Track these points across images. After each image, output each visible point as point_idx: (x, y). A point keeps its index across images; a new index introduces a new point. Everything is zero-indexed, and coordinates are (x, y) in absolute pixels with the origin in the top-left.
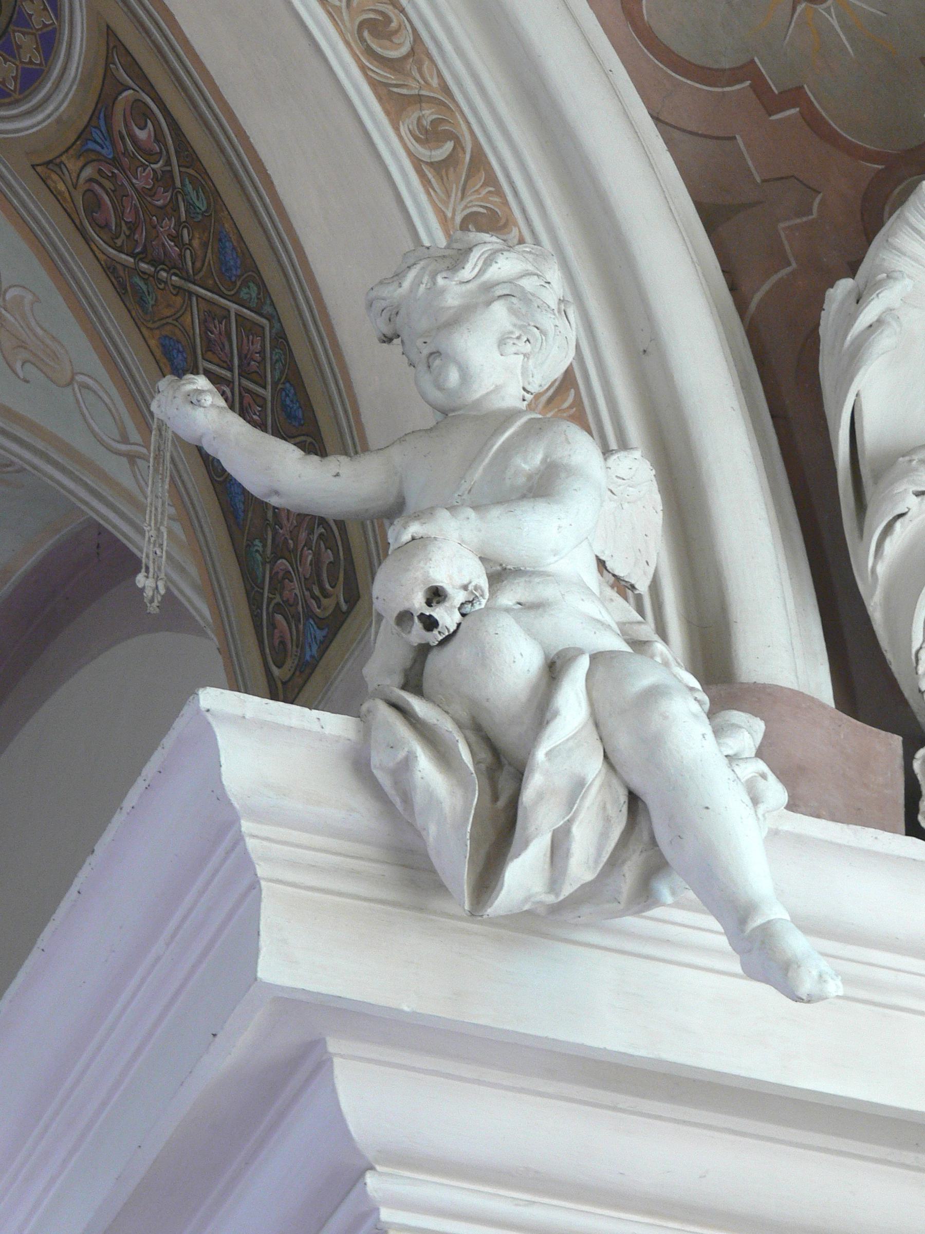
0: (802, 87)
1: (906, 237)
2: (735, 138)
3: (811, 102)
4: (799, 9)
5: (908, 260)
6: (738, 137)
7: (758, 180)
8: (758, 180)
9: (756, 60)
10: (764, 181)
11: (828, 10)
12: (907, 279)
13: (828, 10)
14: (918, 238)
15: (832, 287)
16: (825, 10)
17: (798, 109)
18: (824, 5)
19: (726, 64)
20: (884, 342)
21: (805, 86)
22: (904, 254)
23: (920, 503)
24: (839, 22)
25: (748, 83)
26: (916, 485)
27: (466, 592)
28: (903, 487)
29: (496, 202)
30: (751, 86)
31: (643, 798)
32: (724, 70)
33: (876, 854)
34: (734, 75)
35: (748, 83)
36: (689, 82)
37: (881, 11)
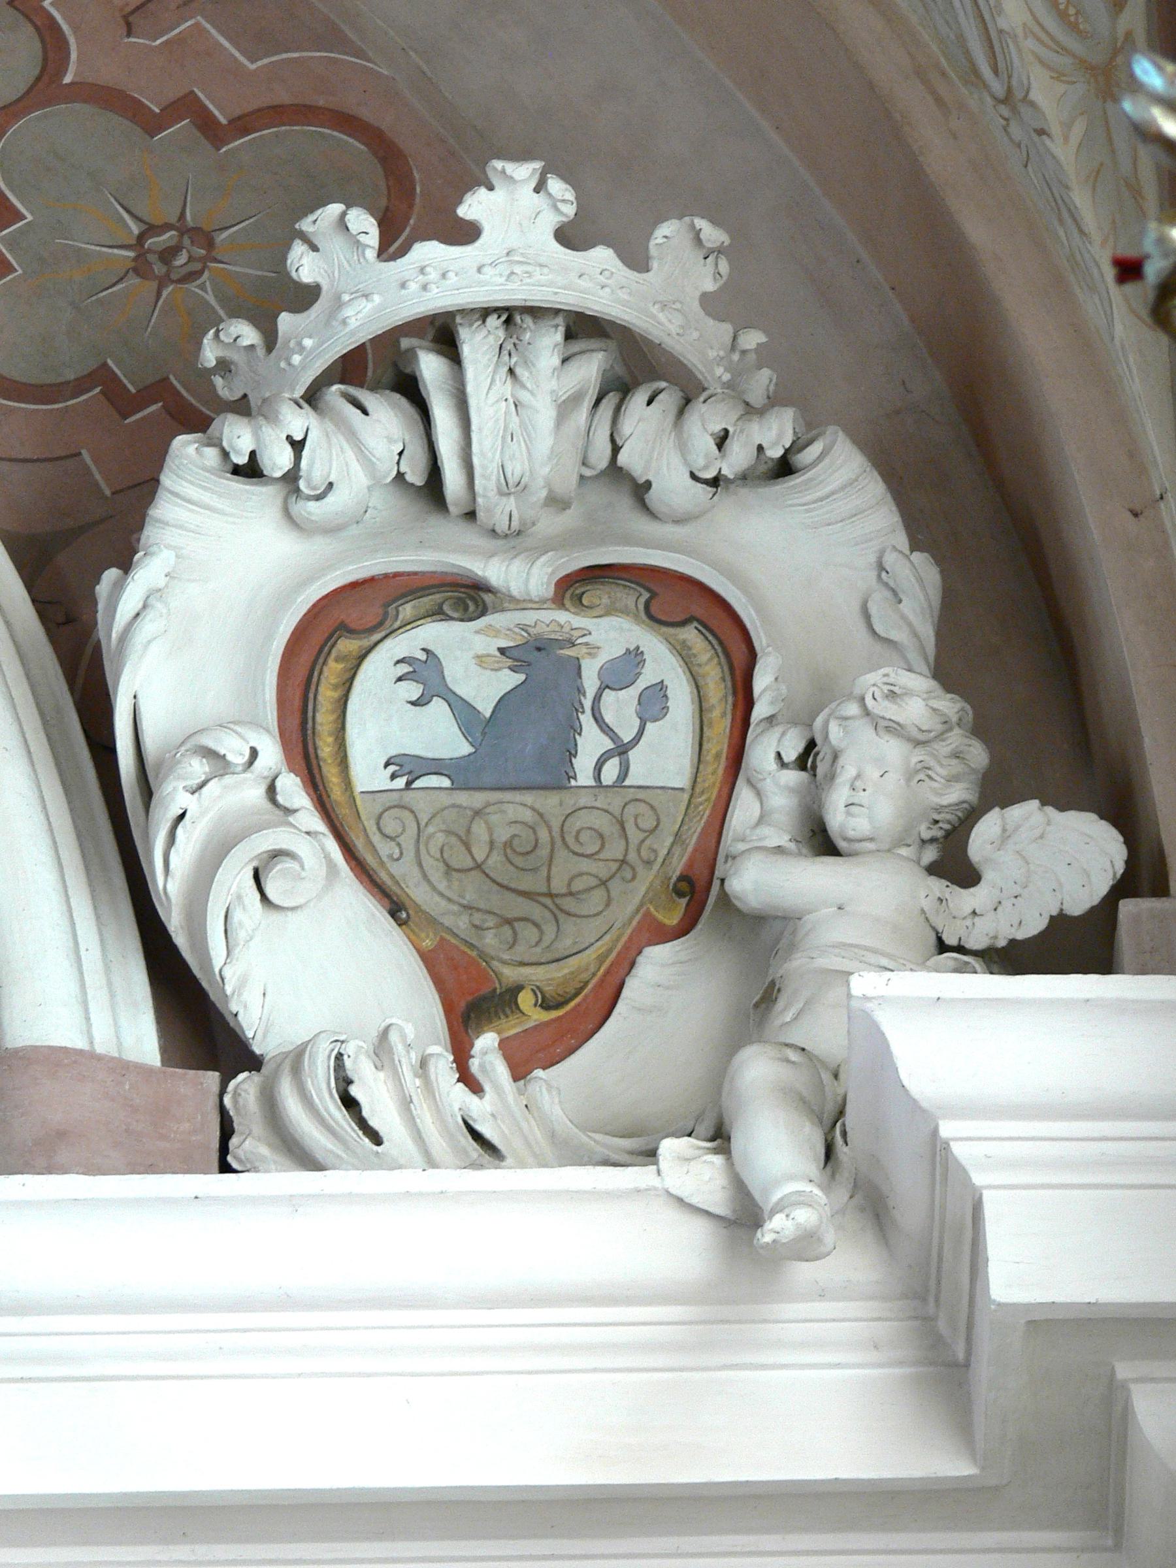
0: (167, 378)
1: (167, 505)
2: (80, 454)
3: (178, 393)
4: (165, 293)
5: (173, 529)
6: (84, 452)
7: (108, 492)
8: (108, 492)
9: (110, 362)
10: (113, 493)
11: (202, 287)
12: (165, 551)
13: (202, 287)
14: (179, 501)
15: (98, 583)
16: (198, 287)
17: (160, 404)
18: (198, 282)
19: (70, 375)
20: (148, 628)
21: (172, 377)
22: (167, 524)
23: (199, 800)
24: (216, 297)
25: (98, 390)
26: (185, 779)
27: (803, 773)
28: (170, 789)
29: (510, 603)
30: (101, 392)
31: (811, 860)
32: (68, 383)
33: (29, 1204)
34: (79, 386)
35: (98, 390)
36: (23, 405)
37: (272, 272)
